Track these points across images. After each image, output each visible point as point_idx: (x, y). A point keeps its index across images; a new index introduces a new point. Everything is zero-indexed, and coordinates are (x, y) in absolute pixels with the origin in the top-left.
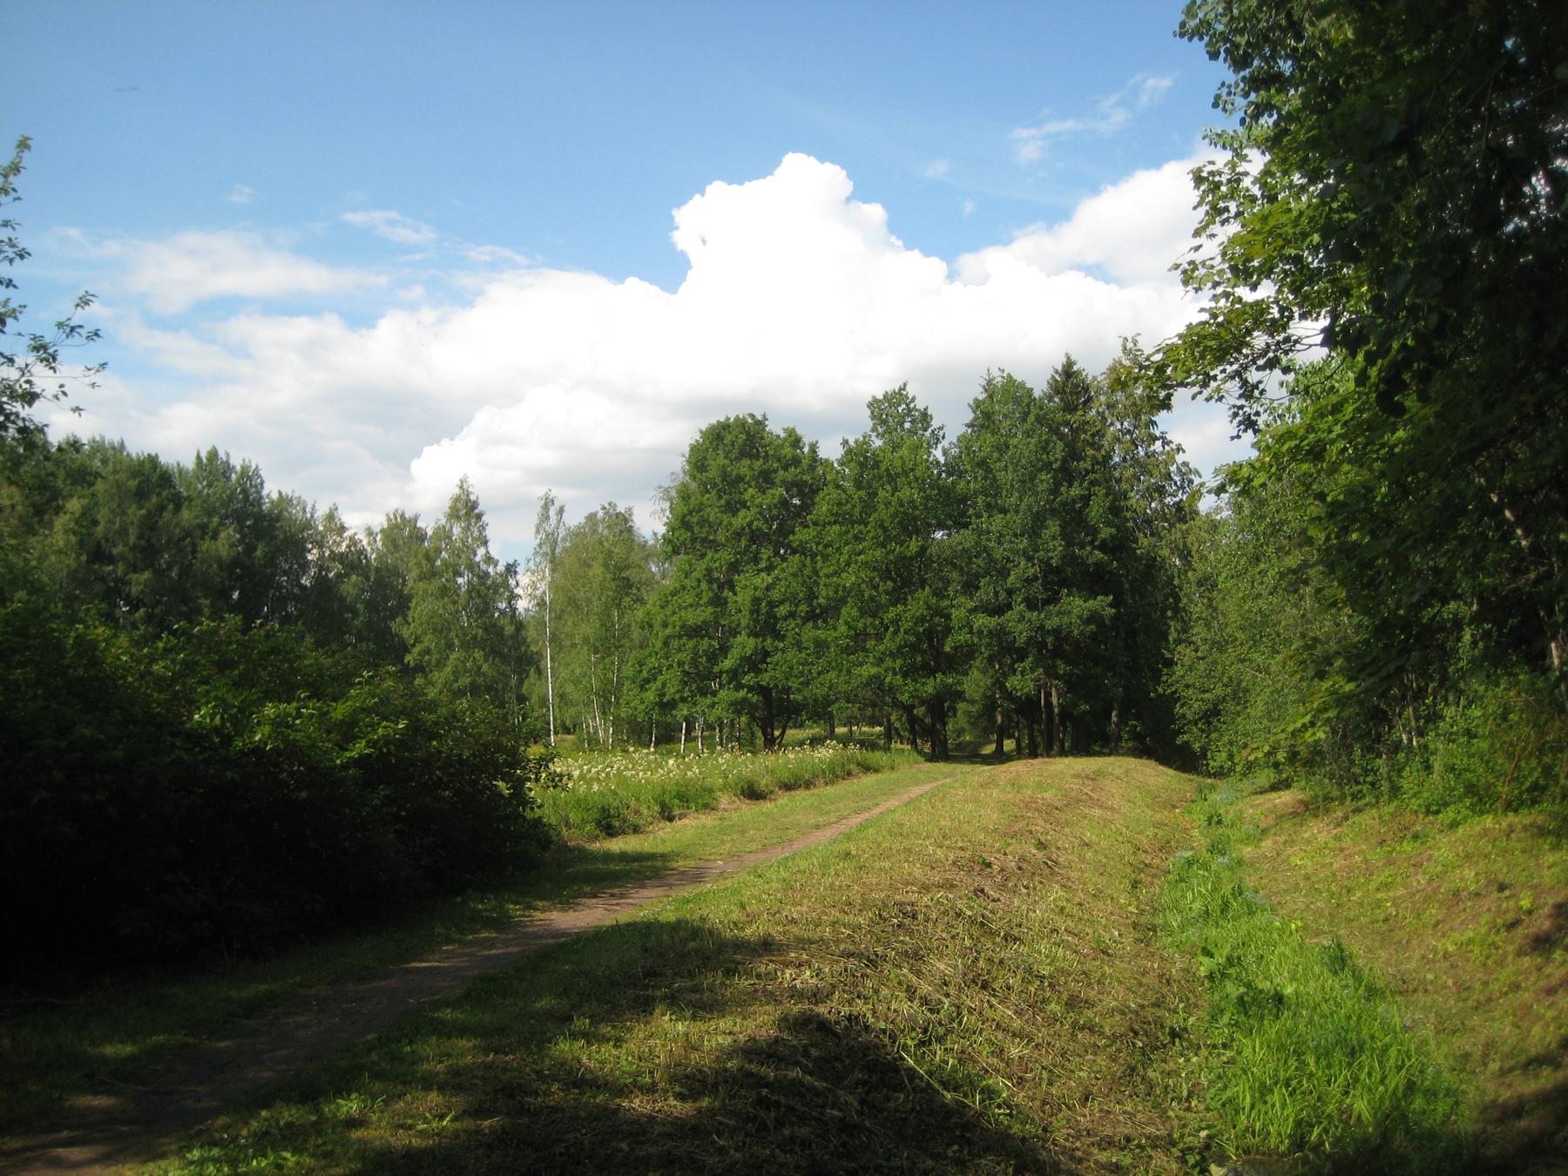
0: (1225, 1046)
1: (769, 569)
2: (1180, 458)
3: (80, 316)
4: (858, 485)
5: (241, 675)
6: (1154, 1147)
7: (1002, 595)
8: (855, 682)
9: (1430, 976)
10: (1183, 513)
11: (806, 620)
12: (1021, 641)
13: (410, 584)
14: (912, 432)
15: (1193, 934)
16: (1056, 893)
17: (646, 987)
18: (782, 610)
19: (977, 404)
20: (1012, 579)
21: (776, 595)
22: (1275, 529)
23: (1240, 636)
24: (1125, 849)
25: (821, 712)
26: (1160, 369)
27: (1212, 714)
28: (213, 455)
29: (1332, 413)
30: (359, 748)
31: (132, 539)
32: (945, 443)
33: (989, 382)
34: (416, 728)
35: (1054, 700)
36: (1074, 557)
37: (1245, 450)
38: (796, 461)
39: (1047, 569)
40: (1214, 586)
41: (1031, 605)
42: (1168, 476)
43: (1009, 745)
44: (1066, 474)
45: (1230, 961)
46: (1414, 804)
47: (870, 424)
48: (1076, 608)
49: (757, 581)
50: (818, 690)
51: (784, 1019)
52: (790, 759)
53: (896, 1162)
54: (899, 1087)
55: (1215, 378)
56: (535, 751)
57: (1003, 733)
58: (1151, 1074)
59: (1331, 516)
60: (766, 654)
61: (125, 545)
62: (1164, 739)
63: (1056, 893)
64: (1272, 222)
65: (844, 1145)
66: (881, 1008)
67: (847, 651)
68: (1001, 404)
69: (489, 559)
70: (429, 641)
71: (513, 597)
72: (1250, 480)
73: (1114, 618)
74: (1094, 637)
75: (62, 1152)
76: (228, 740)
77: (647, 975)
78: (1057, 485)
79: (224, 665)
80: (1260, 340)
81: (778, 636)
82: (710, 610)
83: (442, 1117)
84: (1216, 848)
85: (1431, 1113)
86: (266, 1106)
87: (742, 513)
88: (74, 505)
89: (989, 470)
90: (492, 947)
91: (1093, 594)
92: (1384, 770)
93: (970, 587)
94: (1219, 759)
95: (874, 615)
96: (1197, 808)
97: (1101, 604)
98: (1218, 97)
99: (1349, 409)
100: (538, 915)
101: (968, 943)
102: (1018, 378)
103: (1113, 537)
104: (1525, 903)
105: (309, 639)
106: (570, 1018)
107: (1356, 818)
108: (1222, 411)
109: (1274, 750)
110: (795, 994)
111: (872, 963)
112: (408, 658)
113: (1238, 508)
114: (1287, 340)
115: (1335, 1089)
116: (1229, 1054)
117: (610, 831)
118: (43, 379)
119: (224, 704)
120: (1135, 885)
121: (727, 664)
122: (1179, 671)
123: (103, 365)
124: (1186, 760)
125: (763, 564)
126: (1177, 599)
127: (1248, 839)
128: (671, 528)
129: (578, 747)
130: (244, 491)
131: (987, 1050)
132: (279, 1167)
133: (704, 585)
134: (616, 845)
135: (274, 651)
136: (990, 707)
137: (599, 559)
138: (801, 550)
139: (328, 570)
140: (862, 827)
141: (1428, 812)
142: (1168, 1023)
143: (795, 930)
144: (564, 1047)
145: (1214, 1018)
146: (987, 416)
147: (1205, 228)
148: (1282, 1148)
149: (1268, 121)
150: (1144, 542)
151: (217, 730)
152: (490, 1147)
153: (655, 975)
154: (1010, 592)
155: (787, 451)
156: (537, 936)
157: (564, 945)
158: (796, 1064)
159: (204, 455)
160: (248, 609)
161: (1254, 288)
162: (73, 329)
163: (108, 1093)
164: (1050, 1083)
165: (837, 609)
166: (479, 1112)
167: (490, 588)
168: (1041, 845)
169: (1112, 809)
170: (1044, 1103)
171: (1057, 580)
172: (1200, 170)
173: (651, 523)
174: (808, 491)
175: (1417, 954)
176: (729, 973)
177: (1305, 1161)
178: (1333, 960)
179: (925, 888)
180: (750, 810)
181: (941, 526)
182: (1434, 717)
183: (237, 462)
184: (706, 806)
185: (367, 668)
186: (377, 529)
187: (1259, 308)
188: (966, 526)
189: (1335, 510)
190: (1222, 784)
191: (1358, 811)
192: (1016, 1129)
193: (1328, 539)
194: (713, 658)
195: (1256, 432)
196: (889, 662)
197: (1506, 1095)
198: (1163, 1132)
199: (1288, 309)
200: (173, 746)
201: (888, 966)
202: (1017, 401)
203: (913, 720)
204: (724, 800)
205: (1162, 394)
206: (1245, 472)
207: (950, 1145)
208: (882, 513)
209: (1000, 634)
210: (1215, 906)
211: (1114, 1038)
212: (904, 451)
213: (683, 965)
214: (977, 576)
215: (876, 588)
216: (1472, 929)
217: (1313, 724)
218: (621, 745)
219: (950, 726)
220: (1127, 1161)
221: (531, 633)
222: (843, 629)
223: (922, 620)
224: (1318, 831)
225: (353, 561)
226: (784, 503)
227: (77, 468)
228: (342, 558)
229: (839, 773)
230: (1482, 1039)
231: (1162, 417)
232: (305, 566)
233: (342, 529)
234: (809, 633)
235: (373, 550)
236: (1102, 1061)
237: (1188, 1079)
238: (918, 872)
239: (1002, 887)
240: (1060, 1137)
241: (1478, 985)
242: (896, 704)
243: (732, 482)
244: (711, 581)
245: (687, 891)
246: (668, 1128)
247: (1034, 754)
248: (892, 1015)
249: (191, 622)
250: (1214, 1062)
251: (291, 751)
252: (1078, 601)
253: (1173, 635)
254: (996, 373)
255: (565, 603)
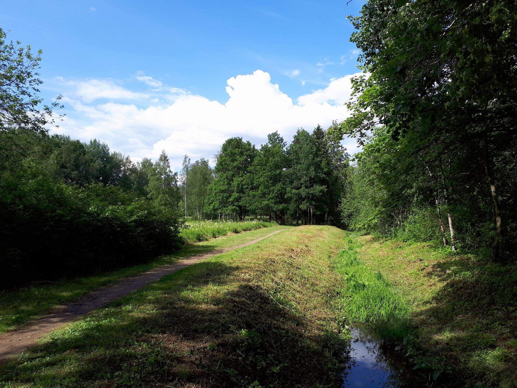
0: (350, 297)
1: (242, 176)
2: (345, 152)
3: (58, 101)
4: (265, 156)
5: (102, 199)
6: (332, 320)
7: (299, 185)
8: (262, 205)
9: (402, 281)
10: (346, 166)
11: (251, 189)
12: (303, 196)
13: (149, 177)
14: (279, 143)
15: (344, 269)
16: (310, 258)
17: (207, 278)
18: (245, 187)
19: (295, 136)
20: (302, 181)
21: (243, 183)
22: (369, 170)
23: (359, 197)
24: (328, 248)
25: (254, 213)
26: (340, 129)
27: (350, 216)
28: (95, 141)
29: (383, 141)
30: (134, 218)
31: (72, 163)
32: (287, 146)
33: (298, 131)
34: (150, 213)
35: (311, 211)
36: (317, 176)
37: (361, 149)
38: (249, 150)
39: (311, 179)
40: (352, 184)
41: (307, 187)
42: (342, 156)
43: (300, 222)
44: (316, 155)
45: (352, 276)
46: (400, 239)
47: (268, 141)
48: (318, 189)
49: (239, 179)
50: (253, 207)
51: (241, 286)
52: (245, 224)
53: (267, 322)
54: (269, 303)
55: (354, 132)
56: (181, 220)
57: (299, 219)
58: (331, 303)
59: (381, 167)
60: (241, 198)
61: (70, 164)
62: (337, 221)
63: (310, 258)
64: (371, 92)
65: (255, 317)
66: (265, 284)
67: (261, 197)
68: (301, 137)
69: (170, 171)
70: (154, 192)
71: (176, 181)
72: (361, 157)
73: (327, 191)
74: (322, 196)
75: (52, 319)
76: (99, 215)
77: (207, 275)
78: (314, 157)
79: (97, 196)
80: (365, 122)
81: (244, 193)
82: (227, 186)
83: (153, 310)
84: (350, 249)
85: (400, 315)
86: (107, 307)
87: (236, 162)
88: (56, 152)
89: (297, 153)
90: (168, 268)
91: (322, 185)
92: (393, 231)
93: (292, 182)
94: (352, 227)
95: (267, 189)
96: (346, 238)
97: (324, 188)
98: (359, 58)
99: (387, 140)
100: (180, 261)
101: (287, 269)
102: (306, 130)
103: (327, 171)
104: (426, 264)
105: (121, 190)
106: (187, 285)
107: (386, 242)
108: (355, 140)
109: (364, 225)
110: (244, 280)
111: (263, 273)
112: (148, 196)
113: (359, 165)
114: (373, 122)
115: (377, 308)
116: (351, 299)
117: (200, 240)
118: (47, 118)
119: (98, 206)
120: (330, 257)
121: (231, 200)
122: (343, 205)
123: (65, 115)
124: (343, 227)
125: (240, 175)
126: (343, 187)
127: (358, 247)
128: (218, 165)
129: (192, 220)
130: (104, 151)
131: (291, 295)
132: (111, 322)
133: (226, 180)
134: (201, 244)
135: (112, 192)
136: (296, 212)
137: (198, 172)
138: (250, 172)
139: (126, 172)
140: (263, 240)
141: (404, 241)
142: (336, 290)
143: (245, 264)
144: (185, 293)
145: (348, 290)
146: (298, 140)
147: (354, 93)
148: (363, 322)
149: (371, 66)
150: (335, 172)
151: (96, 212)
152: (165, 317)
153: (210, 275)
154: (301, 184)
155: (247, 147)
156: (180, 266)
157: (186, 268)
158: (244, 297)
159: (92, 141)
160: (105, 182)
161: (365, 109)
162: (56, 104)
163: (65, 305)
164: (306, 304)
165: (259, 187)
166: (163, 308)
167: (170, 179)
168: (307, 246)
169: (325, 238)
170: (305, 308)
171: (313, 182)
172: (353, 78)
173: (212, 164)
174: (252, 157)
175: (399, 276)
176: (228, 275)
177: (369, 325)
178: (378, 276)
179: (278, 255)
180: (235, 235)
181: (285, 167)
182: (406, 218)
183: (101, 143)
184: (224, 235)
185: (137, 197)
186: (140, 162)
187: (366, 114)
188: (291, 167)
189: (381, 165)
190: (353, 233)
191: (386, 241)
192: (297, 315)
193: (379, 172)
194: (227, 198)
195: (363, 145)
196: (271, 201)
197: (418, 310)
198: (334, 317)
199: (373, 114)
200: (84, 216)
201: (267, 274)
202: (305, 136)
203: (276, 215)
204: (229, 233)
205: (340, 135)
206: (360, 155)
207: (281, 318)
208: (270, 164)
209: (299, 194)
210: (349, 262)
211: (323, 293)
212: (276, 148)
213: (216, 273)
214: (293, 180)
215: (268, 182)
216: (413, 269)
217: (374, 218)
218: (203, 219)
219: (285, 217)
220: (324, 323)
221: (181, 191)
222: (260, 192)
223: (279, 190)
224: (376, 245)
225: (134, 170)
226: (246, 160)
227: (58, 143)
228: (130, 170)
229: (257, 227)
230: (414, 297)
231: (341, 141)
232: (120, 171)
233: (130, 162)
234: (251, 193)
235: (139, 167)
236: (319, 299)
237: (341, 305)
238: (276, 251)
239: (296, 256)
240: (308, 317)
241: (413, 284)
242: (273, 211)
243: (233, 154)
244: (227, 179)
245: (219, 255)
246: (211, 312)
247: (306, 224)
248: (268, 286)
249: (89, 184)
250: (347, 300)
251: (116, 218)
252: (318, 187)
253: (342, 196)
254: (300, 129)
255: (189, 184)
